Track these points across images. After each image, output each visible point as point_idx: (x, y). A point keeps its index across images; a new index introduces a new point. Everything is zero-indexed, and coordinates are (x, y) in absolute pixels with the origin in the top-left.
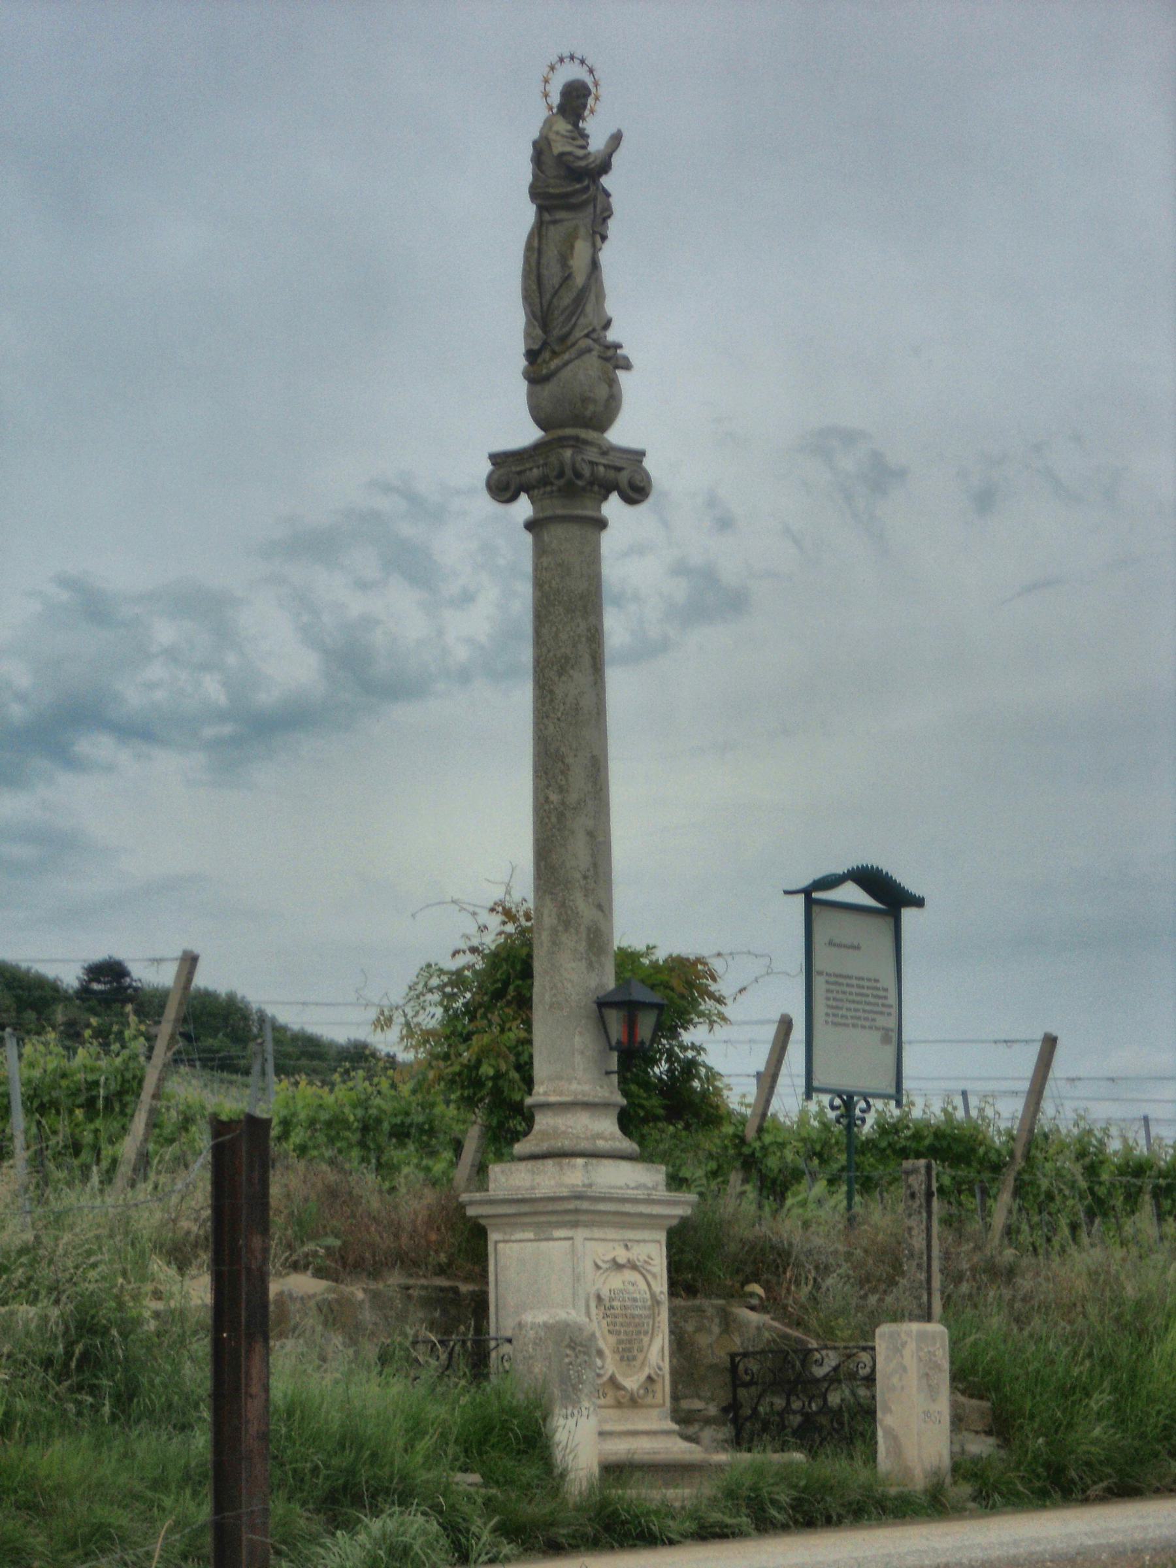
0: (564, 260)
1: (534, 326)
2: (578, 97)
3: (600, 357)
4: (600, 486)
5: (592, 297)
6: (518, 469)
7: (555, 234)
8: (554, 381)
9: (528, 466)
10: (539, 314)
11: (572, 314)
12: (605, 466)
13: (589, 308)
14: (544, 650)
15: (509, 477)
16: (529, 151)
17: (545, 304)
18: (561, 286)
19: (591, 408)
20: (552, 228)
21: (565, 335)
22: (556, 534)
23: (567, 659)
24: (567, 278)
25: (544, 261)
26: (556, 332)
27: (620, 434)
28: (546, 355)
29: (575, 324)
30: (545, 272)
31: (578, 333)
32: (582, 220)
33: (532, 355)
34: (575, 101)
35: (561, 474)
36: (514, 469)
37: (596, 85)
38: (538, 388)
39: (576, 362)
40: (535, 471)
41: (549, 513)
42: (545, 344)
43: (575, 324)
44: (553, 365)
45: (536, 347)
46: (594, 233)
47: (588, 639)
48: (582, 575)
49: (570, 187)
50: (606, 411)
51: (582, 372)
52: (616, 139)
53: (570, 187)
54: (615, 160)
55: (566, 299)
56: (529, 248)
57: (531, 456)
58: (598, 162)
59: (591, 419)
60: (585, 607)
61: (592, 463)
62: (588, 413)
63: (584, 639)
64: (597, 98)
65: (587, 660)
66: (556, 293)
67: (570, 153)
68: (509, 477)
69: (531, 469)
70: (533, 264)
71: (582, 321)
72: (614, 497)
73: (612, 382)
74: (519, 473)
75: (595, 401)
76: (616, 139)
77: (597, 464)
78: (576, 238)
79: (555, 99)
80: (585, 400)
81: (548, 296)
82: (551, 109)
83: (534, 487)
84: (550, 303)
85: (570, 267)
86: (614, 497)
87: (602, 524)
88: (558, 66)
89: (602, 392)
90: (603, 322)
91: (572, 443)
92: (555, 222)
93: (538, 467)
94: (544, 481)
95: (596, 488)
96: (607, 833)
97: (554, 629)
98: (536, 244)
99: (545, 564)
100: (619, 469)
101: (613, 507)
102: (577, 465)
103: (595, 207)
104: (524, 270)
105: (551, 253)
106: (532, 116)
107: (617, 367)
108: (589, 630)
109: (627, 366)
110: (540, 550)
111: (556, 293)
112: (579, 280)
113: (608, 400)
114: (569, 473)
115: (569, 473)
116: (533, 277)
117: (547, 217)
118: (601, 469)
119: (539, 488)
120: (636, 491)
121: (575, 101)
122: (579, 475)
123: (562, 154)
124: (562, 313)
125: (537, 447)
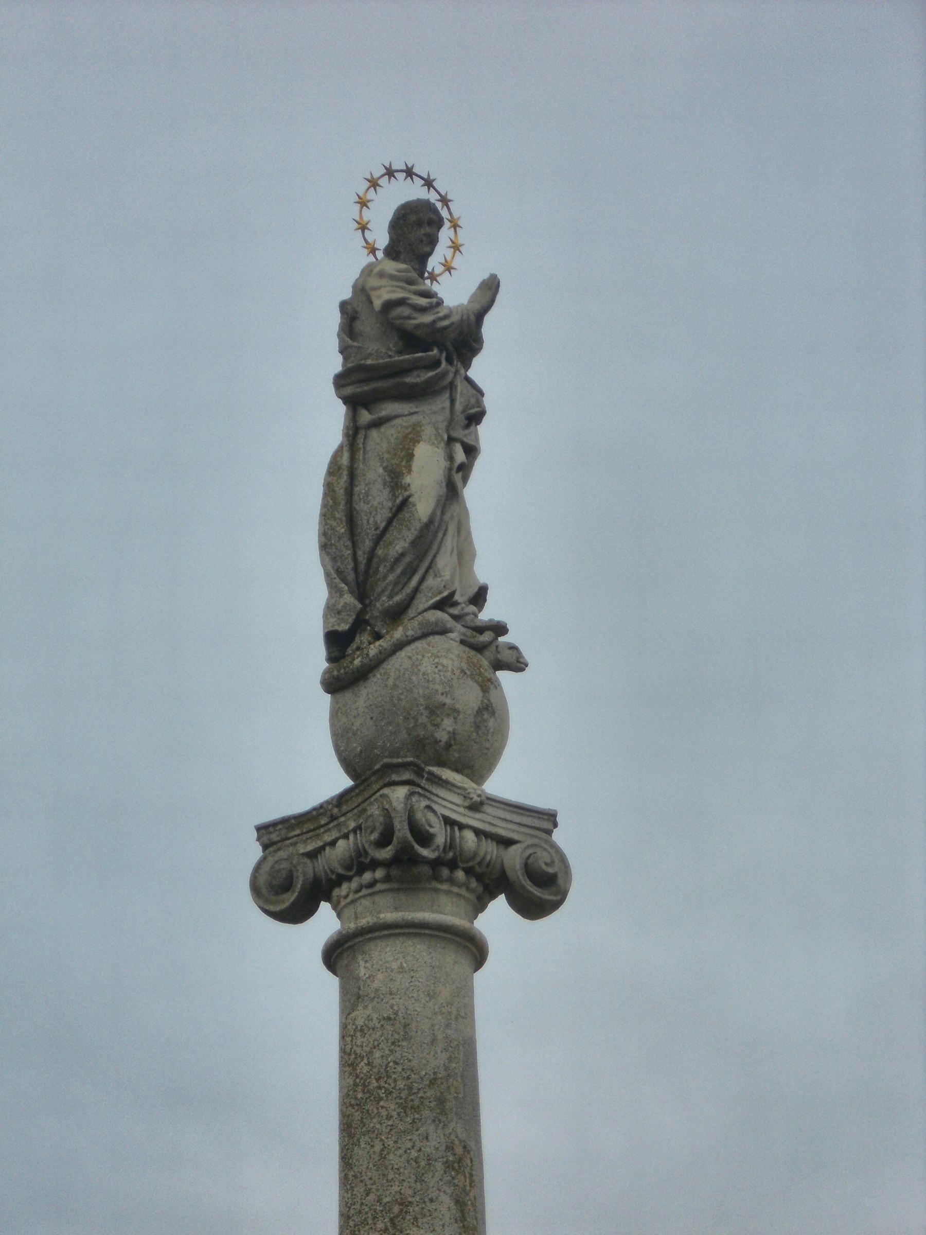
0: (395, 479)
1: (341, 593)
2: (419, 224)
3: (463, 642)
4: (468, 871)
5: (449, 542)
6: (310, 847)
7: (379, 442)
8: (377, 678)
9: (328, 838)
10: (351, 577)
11: (411, 570)
12: (478, 832)
13: (445, 562)
14: (360, 1190)
15: (295, 873)
16: (335, 319)
17: (362, 558)
18: (390, 522)
19: (448, 724)
20: (374, 433)
21: (391, 580)
22: (383, 961)
23: (404, 1203)
24: (402, 507)
25: (360, 488)
26: (384, 602)
27: (506, 781)
28: (363, 638)
29: (416, 590)
30: (361, 506)
31: (422, 602)
32: (431, 415)
33: (338, 643)
34: (416, 231)
35: (385, 839)
36: (302, 849)
37: (445, 201)
38: (348, 695)
39: (418, 645)
40: (341, 843)
41: (366, 921)
42: (359, 623)
43: (416, 590)
44: (373, 650)
45: (344, 627)
46: (451, 440)
47: (448, 1166)
48: (434, 1041)
49: (408, 359)
50: (476, 745)
51: (431, 664)
52: (490, 289)
53: (408, 359)
54: (490, 328)
55: (399, 542)
56: (334, 469)
57: (333, 818)
58: (455, 318)
59: (448, 746)
60: (441, 1101)
61: (449, 822)
62: (442, 736)
63: (439, 1166)
64: (455, 226)
65: (445, 1205)
66: (379, 539)
67: (401, 302)
68: (295, 873)
69: (333, 843)
70: (341, 493)
71: (430, 581)
72: (499, 905)
73: (487, 685)
74: (313, 855)
75: (454, 712)
76: (490, 289)
77: (462, 827)
78: (416, 441)
79: (381, 238)
80: (435, 710)
81: (368, 544)
82: (373, 251)
83: (340, 880)
84: (372, 554)
85: (406, 487)
86: (499, 905)
87: (476, 951)
88: (384, 181)
89: (468, 696)
90: (473, 590)
91: (406, 776)
92: (377, 424)
93: (346, 836)
94: (359, 863)
95: (460, 875)
96: (342, 1138)
97: (378, 1147)
98: (345, 460)
99: (360, 1022)
100: (507, 843)
101: (497, 920)
102: (419, 816)
103: (452, 401)
104: (324, 505)
105: (373, 473)
106: (338, 262)
107: (499, 665)
108: (450, 1148)
109: (518, 665)
110: (352, 998)
111: (379, 539)
112: (423, 508)
113: (480, 712)
114: (402, 830)
115: (402, 830)
116: (340, 514)
117: (365, 417)
118: (469, 836)
119: (349, 879)
120: (539, 891)
121: (416, 231)
122: (425, 839)
123: (389, 305)
124: (392, 569)
125: (342, 798)
